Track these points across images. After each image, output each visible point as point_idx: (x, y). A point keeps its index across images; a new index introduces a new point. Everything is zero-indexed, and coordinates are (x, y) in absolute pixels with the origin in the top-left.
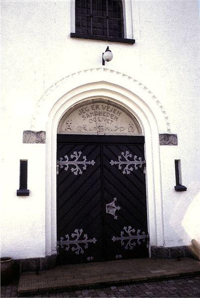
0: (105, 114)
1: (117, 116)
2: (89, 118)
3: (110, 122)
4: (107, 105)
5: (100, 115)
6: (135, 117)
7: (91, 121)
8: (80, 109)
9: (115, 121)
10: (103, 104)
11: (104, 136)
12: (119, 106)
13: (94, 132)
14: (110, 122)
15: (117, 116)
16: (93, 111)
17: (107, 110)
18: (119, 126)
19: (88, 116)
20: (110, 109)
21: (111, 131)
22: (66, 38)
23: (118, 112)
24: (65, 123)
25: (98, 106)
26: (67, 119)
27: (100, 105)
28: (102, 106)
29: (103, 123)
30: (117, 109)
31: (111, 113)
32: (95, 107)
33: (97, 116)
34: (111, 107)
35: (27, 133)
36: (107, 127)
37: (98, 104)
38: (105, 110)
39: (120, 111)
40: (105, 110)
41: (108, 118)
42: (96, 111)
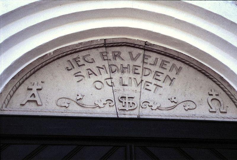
0: (140, 70)
1: (172, 75)
2: (93, 78)
3: (152, 87)
4: (142, 52)
5: (123, 72)
6: (222, 78)
7: (98, 85)
8: (70, 58)
9: (166, 85)
10: (132, 49)
11: (139, 121)
12: (176, 54)
13: (108, 112)
14: (152, 87)
15: (172, 75)
16: (106, 63)
17: (144, 62)
18: (180, 99)
19: (91, 73)
20: (151, 60)
21: (158, 108)
22: (121, 51)
23: (174, 65)
24: (22, 89)
25: (119, 53)
26: (32, 79)
27: (125, 52)
28: (130, 53)
29: (131, 90)
30: (168, 59)
31: (157, 68)
32: (110, 55)
33: (116, 76)
34: (154, 56)
35: (21, 104)
36: (143, 99)
37: (117, 49)
38: (139, 62)
39: (178, 64)
40: (139, 62)
41: (145, 79)
42: (113, 62)
